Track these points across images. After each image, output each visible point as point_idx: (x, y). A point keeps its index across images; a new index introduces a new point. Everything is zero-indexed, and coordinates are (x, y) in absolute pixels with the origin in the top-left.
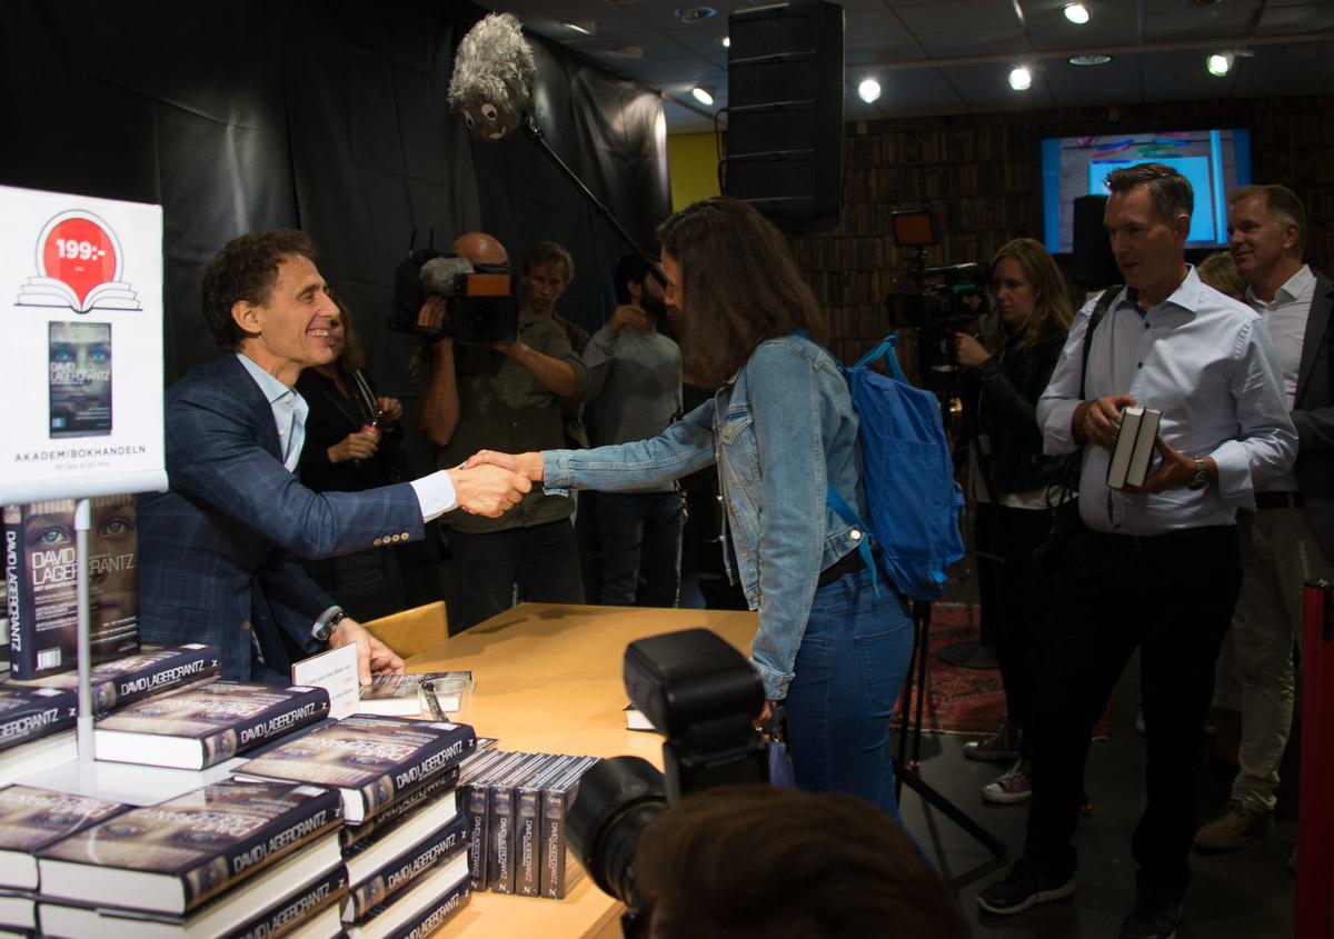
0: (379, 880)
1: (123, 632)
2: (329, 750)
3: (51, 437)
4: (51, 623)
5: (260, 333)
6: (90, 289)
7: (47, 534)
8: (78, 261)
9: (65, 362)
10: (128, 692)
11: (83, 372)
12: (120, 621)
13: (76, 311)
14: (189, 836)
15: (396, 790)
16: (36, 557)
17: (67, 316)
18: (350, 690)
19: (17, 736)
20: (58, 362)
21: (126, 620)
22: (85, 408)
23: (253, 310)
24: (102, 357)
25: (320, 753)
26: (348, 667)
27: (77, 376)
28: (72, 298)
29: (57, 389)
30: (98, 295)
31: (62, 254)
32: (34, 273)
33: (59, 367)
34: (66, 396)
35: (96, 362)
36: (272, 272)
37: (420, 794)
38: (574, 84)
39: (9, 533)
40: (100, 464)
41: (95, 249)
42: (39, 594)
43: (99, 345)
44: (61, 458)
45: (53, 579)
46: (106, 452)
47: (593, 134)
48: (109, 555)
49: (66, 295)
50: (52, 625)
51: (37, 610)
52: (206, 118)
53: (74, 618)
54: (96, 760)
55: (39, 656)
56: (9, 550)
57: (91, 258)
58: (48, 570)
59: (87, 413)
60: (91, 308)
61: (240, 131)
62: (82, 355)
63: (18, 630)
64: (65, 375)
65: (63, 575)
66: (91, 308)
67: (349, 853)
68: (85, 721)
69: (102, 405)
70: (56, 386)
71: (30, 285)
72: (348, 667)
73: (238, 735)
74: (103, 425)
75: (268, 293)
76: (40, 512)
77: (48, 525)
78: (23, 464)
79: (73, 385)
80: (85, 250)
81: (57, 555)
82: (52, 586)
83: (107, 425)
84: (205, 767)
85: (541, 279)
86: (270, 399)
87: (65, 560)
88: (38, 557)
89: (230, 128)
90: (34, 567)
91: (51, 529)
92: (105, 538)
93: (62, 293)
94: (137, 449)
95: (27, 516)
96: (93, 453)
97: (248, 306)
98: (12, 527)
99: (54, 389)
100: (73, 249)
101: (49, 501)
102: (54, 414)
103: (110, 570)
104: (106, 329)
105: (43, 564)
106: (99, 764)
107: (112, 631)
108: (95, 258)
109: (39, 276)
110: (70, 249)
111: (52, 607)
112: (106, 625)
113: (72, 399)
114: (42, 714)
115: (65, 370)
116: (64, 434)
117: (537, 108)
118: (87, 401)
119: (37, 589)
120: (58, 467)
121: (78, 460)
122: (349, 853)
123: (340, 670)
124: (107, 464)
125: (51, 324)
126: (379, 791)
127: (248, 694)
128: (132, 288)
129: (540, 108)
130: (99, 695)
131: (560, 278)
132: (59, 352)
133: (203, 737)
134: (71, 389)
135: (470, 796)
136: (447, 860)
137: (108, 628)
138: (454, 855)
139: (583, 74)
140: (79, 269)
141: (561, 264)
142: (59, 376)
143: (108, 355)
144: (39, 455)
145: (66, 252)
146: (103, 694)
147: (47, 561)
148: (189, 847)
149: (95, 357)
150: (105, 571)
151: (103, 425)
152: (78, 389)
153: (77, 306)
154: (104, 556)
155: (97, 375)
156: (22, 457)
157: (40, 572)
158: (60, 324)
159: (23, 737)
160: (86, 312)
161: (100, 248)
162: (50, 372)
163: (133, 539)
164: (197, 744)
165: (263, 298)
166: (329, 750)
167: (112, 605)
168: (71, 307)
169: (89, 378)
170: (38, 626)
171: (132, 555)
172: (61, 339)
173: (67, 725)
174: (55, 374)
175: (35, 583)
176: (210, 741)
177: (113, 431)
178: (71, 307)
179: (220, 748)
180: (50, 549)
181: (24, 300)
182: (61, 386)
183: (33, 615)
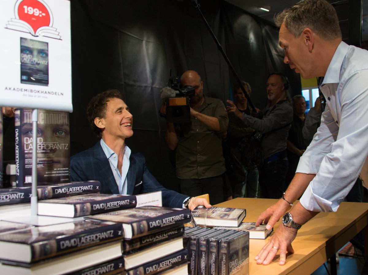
0: (141, 269)
6: (40, 27)
8: (33, 15)
9: (27, 54)
10: (58, 192)
11: (35, 59)
13: (33, 35)
15: (149, 229)
16: (26, 139)
17: (29, 37)
21: (65, 169)
23: (101, 120)
24: (44, 55)
27: (33, 61)
28: (30, 29)
29: (24, 64)
30: (42, 32)
31: (26, 12)
32: (14, 17)
33: (25, 56)
34: (28, 68)
35: (41, 57)
37: (165, 235)
38: (264, 31)
39: (16, 130)
40: (43, 97)
41: (41, 12)
42: (27, 153)
44: (26, 91)
46: (46, 92)
47: (272, 50)
48: (57, 143)
51: (26, 160)
52: (136, 38)
53: (30, 159)
54: (38, 215)
55: (26, 178)
56: (16, 136)
57: (39, 16)
58: (31, 145)
59: (37, 76)
61: (147, 42)
62: (35, 53)
63: (18, 167)
64: (27, 59)
67: (126, 253)
68: (34, 199)
70: (23, 63)
71: (12, 21)
74: (45, 82)
76: (28, 122)
78: (8, 91)
79: (32, 64)
80: (37, 12)
83: (47, 82)
84: (75, 216)
88: (27, 140)
89: (144, 42)
90: (25, 143)
92: (57, 136)
93: (22, 25)
94: (60, 94)
95: (23, 123)
96: (40, 92)
97: (99, 119)
98: (17, 127)
99: (23, 64)
103: (58, 149)
104: (46, 45)
106: (40, 217)
107: (58, 172)
109: (16, 18)
110: (29, 10)
112: (55, 169)
113: (30, 69)
114: (16, 194)
115: (27, 58)
116: (27, 82)
117: (250, 39)
118: (38, 71)
120: (24, 95)
121: (33, 94)
122: (126, 253)
126: (140, 226)
128: (60, 35)
129: (251, 39)
130: (45, 192)
132: (24, 50)
133: (75, 204)
135: (190, 242)
136: (177, 267)
138: (180, 266)
139: (267, 28)
140: (34, 19)
142: (25, 59)
143: (47, 55)
144: (16, 89)
145: (28, 11)
146: (46, 191)
147: (30, 141)
149: (41, 55)
150: (56, 149)
151: (45, 82)
152: (34, 66)
153: (33, 33)
154: (55, 143)
155: (42, 62)
156: (8, 89)
157: (28, 145)
158: (26, 39)
159: (6, 202)
162: (21, 57)
164: (72, 207)
167: (58, 162)
168: (30, 33)
169: (38, 62)
170: (26, 166)
171: (67, 144)
173: (26, 201)
174: (23, 58)
175: (25, 149)
176: (78, 206)
178: (30, 33)
179: (82, 209)
181: (9, 27)
182: (26, 63)
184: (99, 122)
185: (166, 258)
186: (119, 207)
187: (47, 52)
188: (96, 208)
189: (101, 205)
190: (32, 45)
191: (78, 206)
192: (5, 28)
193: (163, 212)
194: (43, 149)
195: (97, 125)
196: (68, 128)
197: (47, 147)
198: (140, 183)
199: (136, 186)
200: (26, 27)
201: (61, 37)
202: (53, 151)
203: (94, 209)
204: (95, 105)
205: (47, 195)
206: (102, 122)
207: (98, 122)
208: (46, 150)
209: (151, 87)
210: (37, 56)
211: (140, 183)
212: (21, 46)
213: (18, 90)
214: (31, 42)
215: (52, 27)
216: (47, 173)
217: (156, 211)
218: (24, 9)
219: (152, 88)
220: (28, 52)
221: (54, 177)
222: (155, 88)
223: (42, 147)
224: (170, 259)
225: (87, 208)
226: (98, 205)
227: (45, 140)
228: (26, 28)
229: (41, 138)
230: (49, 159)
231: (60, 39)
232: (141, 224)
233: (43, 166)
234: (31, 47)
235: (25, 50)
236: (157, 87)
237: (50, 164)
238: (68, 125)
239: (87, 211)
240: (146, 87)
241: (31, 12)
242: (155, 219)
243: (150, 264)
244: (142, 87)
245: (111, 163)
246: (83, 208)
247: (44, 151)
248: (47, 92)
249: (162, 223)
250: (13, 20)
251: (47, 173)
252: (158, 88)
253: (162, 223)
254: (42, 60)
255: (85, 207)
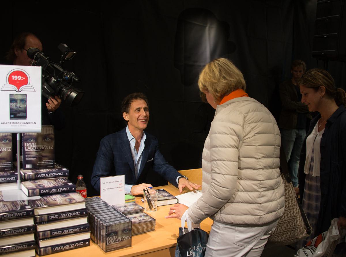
1: (49, 163)
3: (10, 119)
4: (29, 159)
7: (29, 139)
8: (17, 80)
9: (14, 103)
11: (19, 105)
12: (6, 163)
13: (17, 92)
17: (15, 93)
19: (3, 181)
20: (12, 103)
22: (19, 113)
30: (24, 88)
31: (13, 79)
32: (6, 83)
33: (12, 104)
34: (14, 110)
40: (23, 126)
42: (26, 152)
43: (23, 99)
44: (13, 124)
45: (30, 149)
46: (25, 123)
48: (3, 147)
49: (14, 88)
50: (29, 159)
51: (26, 155)
55: (26, 165)
57: (21, 80)
58: (29, 147)
60: (21, 91)
62: (19, 101)
65: (33, 148)
66: (21, 91)
68: (19, 181)
69: (24, 113)
74: (25, 117)
77: (29, 137)
80: (20, 78)
81: (31, 144)
82: (30, 151)
85: (296, 71)
87: (33, 145)
88: (27, 144)
91: (30, 138)
92: (2, 143)
93: (13, 87)
94: (34, 123)
95: (24, 135)
96: (21, 123)
100: (15, 78)
101: (31, 133)
102: (11, 114)
103: (46, 149)
104: (25, 96)
105: (28, 145)
107: (3, 165)
108: (22, 79)
109: (7, 84)
110: (15, 77)
111: (30, 155)
112: (44, 161)
113: (16, 111)
115: (14, 105)
118: (21, 111)
119: (26, 151)
120: (12, 126)
121: (17, 125)
124: (25, 126)
125: (10, 94)
131: (302, 70)
132: (12, 100)
134: (15, 109)
137: (44, 161)
140: (18, 82)
141: (302, 66)
142: (12, 106)
143: (26, 101)
145: (14, 78)
149: (22, 102)
151: (25, 117)
152: (18, 109)
153: (17, 90)
155: (23, 106)
157: (27, 147)
160: (20, 92)
161: (23, 77)
163: (53, 142)
167: (46, 157)
168: (16, 91)
169: (20, 106)
171: (10, 148)
172: (13, 98)
173: (16, 181)
174: (11, 105)
176: (30, 191)
177: (27, 118)
178: (16, 91)
179: (33, 193)
180: (30, 142)
181: (3, 89)
182: (13, 108)
183: (25, 156)
185: (70, 228)
187: (25, 100)
190: (17, 97)
191: (30, 191)
192: (1, 90)
194: (37, 149)
196: (53, 136)
197: (39, 148)
198: (151, 160)
199: (148, 161)
200: (13, 87)
201: (35, 89)
202: (43, 150)
203: (42, 193)
205: (31, 178)
208: (38, 150)
210: (20, 103)
211: (151, 160)
212: (10, 99)
213: (9, 123)
214: (16, 95)
215: (29, 85)
216: (38, 163)
218: (12, 77)
220: (14, 102)
221: (43, 165)
223: (36, 148)
224: (73, 229)
225: (37, 192)
227: (37, 144)
228: (12, 88)
229: (35, 143)
230: (40, 155)
231: (34, 91)
233: (37, 158)
234: (16, 98)
235: (12, 101)
237: (40, 158)
238: (53, 134)
241: (16, 79)
243: (56, 230)
245: (257, 102)
246: (34, 192)
247: (37, 150)
248: (26, 123)
250: (6, 85)
251: (38, 163)
254: (23, 105)
255: (35, 192)
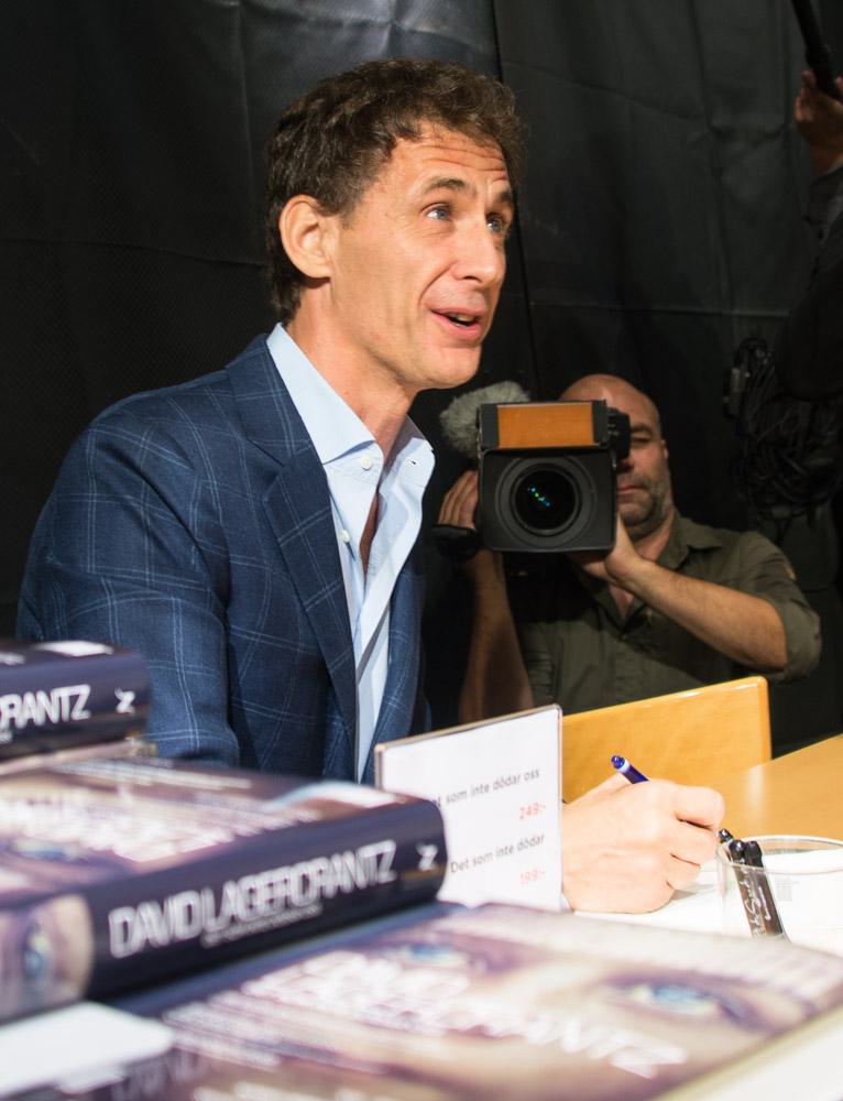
2: (553, 999)
5: (326, 280)
14: (471, 963)
18: (538, 840)
23: (322, 221)
25: (587, 989)
26: (534, 775)
36: (379, 152)
72: (534, 775)
73: (100, 927)
75: (358, 193)
86: (325, 452)
97: (317, 211)
123: (514, 780)
127: (185, 796)
148: (475, 939)
165: (346, 201)
166: (553, 999)
184: (311, 228)
186: (313, 910)
188: (137, 941)
189: (177, 905)
193: (234, 819)
195: (289, 237)
204: (334, 120)
206: (321, 238)
207: (299, 227)
209: (390, 26)
217: (185, 810)
219: (396, 35)
222: (413, 32)
226: (149, 912)
232: (31, 930)
236: (425, 28)
239: (60, 974)
240: (362, 26)
242: (156, 885)
244: (338, 25)
249: (218, 912)
252: (429, 34)
253: (218, 912)
255: (41, 943)
